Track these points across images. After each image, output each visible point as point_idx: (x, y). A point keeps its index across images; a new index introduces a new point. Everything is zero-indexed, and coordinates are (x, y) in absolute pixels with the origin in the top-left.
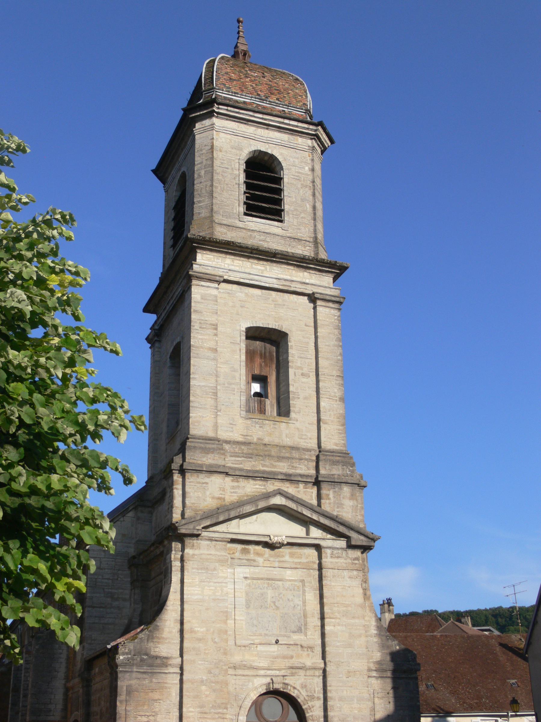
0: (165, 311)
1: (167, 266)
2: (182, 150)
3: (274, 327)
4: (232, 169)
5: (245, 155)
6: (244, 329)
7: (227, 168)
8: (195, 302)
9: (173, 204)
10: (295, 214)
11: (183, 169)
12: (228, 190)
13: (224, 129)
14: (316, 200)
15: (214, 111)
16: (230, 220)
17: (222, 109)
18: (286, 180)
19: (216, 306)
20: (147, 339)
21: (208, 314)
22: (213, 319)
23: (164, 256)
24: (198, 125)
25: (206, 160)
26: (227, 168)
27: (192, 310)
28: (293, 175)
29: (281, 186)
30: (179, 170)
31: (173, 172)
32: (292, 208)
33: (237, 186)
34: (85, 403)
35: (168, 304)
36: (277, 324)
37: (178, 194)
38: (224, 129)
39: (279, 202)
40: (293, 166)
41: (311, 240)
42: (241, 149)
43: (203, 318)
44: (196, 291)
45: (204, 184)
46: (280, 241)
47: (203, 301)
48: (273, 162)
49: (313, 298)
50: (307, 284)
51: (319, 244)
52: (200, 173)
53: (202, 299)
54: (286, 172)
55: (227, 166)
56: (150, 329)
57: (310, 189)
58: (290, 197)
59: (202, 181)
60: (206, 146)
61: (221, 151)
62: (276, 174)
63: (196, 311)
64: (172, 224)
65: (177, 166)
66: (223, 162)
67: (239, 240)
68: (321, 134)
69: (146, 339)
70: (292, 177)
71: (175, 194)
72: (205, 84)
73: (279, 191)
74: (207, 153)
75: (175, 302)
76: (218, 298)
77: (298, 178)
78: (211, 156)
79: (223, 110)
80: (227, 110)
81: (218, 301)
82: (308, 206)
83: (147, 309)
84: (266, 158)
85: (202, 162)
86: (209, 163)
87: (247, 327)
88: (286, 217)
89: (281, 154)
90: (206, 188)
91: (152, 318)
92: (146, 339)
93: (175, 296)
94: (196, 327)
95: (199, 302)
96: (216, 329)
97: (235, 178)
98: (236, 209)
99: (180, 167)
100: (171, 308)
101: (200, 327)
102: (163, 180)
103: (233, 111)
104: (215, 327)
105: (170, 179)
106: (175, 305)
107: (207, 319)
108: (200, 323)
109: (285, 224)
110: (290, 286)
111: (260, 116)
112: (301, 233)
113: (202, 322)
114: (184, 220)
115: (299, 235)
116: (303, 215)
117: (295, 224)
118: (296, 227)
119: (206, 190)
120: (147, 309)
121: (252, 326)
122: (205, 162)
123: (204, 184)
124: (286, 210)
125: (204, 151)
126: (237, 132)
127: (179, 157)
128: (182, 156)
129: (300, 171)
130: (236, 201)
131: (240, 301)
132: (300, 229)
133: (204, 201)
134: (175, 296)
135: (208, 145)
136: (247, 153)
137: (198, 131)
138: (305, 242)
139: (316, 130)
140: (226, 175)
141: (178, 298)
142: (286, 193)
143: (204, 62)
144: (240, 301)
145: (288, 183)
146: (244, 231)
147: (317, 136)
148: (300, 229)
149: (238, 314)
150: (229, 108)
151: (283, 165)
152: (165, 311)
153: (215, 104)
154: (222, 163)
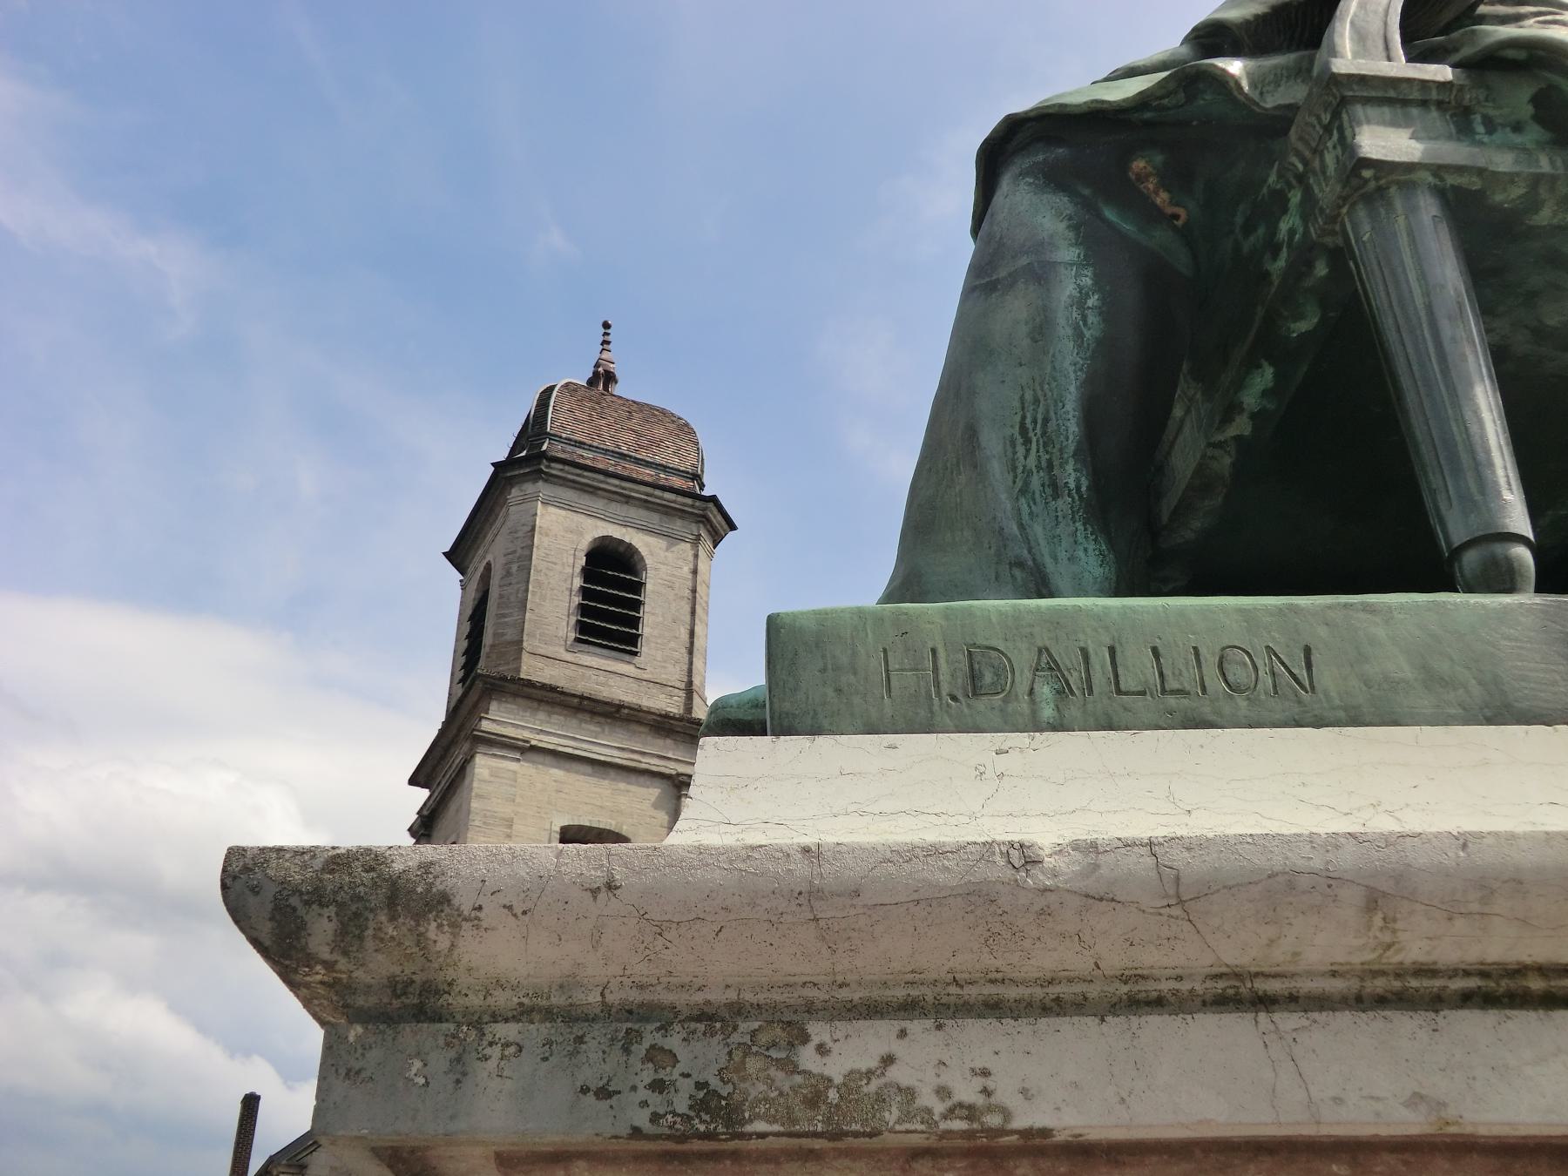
0: (440, 788)
1: (453, 705)
2: (492, 525)
3: (608, 828)
4: (563, 564)
5: (585, 544)
6: (558, 829)
7: (555, 564)
8: (479, 780)
9: (469, 612)
10: (659, 641)
11: (489, 558)
12: (553, 599)
13: (556, 499)
14: (697, 621)
15: (541, 471)
16: (551, 648)
17: (554, 469)
18: (649, 587)
19: (514, 789)
20: (410, 830)
21: (499, 801)
22: (506, 810)
23: (450, 694)
24: (515, 492)
25: (523, 548)
26: (555, 564)
27: (473, 794)
28: (662, 579)
29: (640, 596)
30: (484, 558)
31: (476, 559)
32: (656, 633)
33: (568, 593)
34: (1448, 125)
35: (444, 776)
36: (614, 823)
37: (479, 595)
38: (556, 499)
39: (635, 622)
40: (664, 564)
41: (683, 686)
42: (581, 534)
43: (489, 808)
44: (483, 762)
45: (516, 587)
46: (632, 685)
47: (492, 779)
48: (632, 556)
49: (676, 781)
50: (669, 759)
51: (695, 693)
52: (511, 568)
53: (492, 776)
54: (650, 573)
55: (554, 560)
56: (418, 813)
57: (688, 603)
58: (653, 614)
59: (513, 582)
60: (523, 525)
61: (547, 535)
62: (636, 577)
63: (479, 796)
64: (465, 644)
65: (481, 552)
66: (549, 553)
67: (562, 683)
68: (715, 517)
69: (409, 830)
70: (660, 581)
71: (473, 594)
72: (533, 426)
73: (637, 605)
74: (524, 537)
75: (453, 776)
76: (518, 775)
77: (670, 584)
78: (529, 542)
79: (556, 469)
80: (561, 470)
81: (518, 780)
82: (682, 630)
83: (414, 781)
84: (622, 549)
85: (515, 552)
86: (525, 553)
87: (563, 825)
88: (645, 648)
89: (647, 545)
90: (518, 593)
91: (421, 795)
92: (409, 830)
93: (454, 766)
94: (477, 823)
95: (485, 781)
96: (510, 827)
97: (566, 580)
98: (563, 631)
99: (486, 552)
100: (448, 784)
101: (484, 823)
102: (462, 570)
103: (571, 474)
104: (509, 823)
105: (470, 570)
106: (453, 780)
107: (496, 809)
108: (485, 816)
109: (642, 658)
110: (640, 762)
111: (616, 482)
112: (666, 674)
113: (488, 814)
114: (481, 641)
115: (662, 678)
116: (672, 644)
117: (659, 659)
118: (659, 664)
119: (517, 597)
120: (414, 781)
121: (572, 824)
122: (519, 551)
123: (516, 587)
124: (645, 635)
125: (520, 534)
126: (577, 505)
127: (485, 537)
128: (490, 537)
129: (675, 573)
130: (564, 617)
131: (555, 781)
132: (665, 667)
133: (511, 615)
134: (454, 766)
135: (527, 525)
136: (591, 540)
137: (514, 500)
138: (671, 689)
139: (704, 509)
140: (551, 574)
141: (457, 769)
142: (647, 608)
143: (564, 378)
144: (555, 781)
145: (653, 592)
146: (573, 667)
147: (704, 516)
148: (665, 667)
149: (549, 803)
150: (567, 468)
151: (647, 562)
152: (440, 788)
153: (544, 461)
154: (547, 555)
